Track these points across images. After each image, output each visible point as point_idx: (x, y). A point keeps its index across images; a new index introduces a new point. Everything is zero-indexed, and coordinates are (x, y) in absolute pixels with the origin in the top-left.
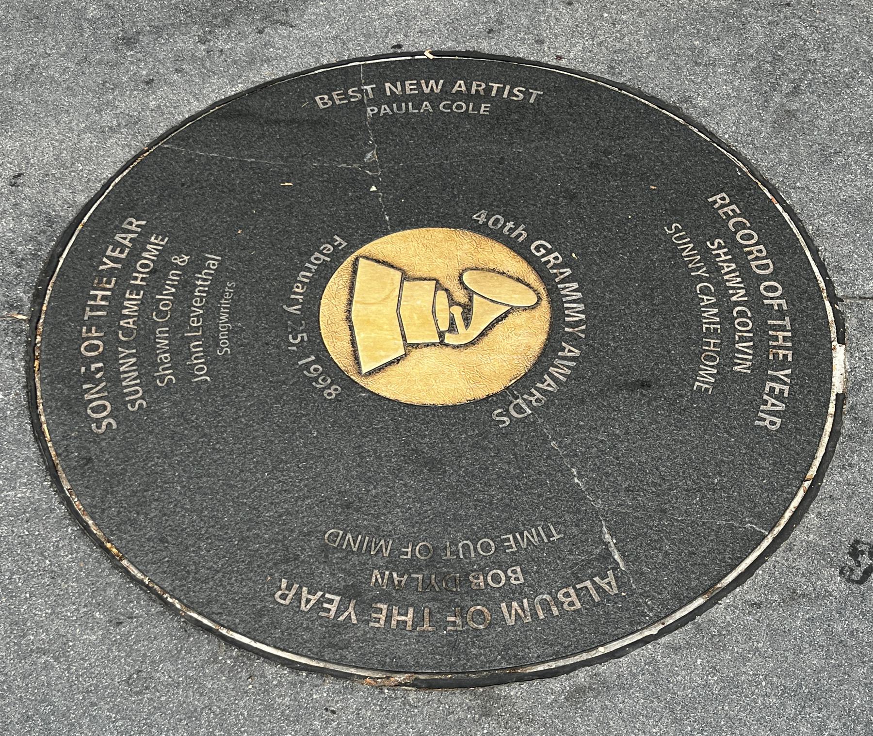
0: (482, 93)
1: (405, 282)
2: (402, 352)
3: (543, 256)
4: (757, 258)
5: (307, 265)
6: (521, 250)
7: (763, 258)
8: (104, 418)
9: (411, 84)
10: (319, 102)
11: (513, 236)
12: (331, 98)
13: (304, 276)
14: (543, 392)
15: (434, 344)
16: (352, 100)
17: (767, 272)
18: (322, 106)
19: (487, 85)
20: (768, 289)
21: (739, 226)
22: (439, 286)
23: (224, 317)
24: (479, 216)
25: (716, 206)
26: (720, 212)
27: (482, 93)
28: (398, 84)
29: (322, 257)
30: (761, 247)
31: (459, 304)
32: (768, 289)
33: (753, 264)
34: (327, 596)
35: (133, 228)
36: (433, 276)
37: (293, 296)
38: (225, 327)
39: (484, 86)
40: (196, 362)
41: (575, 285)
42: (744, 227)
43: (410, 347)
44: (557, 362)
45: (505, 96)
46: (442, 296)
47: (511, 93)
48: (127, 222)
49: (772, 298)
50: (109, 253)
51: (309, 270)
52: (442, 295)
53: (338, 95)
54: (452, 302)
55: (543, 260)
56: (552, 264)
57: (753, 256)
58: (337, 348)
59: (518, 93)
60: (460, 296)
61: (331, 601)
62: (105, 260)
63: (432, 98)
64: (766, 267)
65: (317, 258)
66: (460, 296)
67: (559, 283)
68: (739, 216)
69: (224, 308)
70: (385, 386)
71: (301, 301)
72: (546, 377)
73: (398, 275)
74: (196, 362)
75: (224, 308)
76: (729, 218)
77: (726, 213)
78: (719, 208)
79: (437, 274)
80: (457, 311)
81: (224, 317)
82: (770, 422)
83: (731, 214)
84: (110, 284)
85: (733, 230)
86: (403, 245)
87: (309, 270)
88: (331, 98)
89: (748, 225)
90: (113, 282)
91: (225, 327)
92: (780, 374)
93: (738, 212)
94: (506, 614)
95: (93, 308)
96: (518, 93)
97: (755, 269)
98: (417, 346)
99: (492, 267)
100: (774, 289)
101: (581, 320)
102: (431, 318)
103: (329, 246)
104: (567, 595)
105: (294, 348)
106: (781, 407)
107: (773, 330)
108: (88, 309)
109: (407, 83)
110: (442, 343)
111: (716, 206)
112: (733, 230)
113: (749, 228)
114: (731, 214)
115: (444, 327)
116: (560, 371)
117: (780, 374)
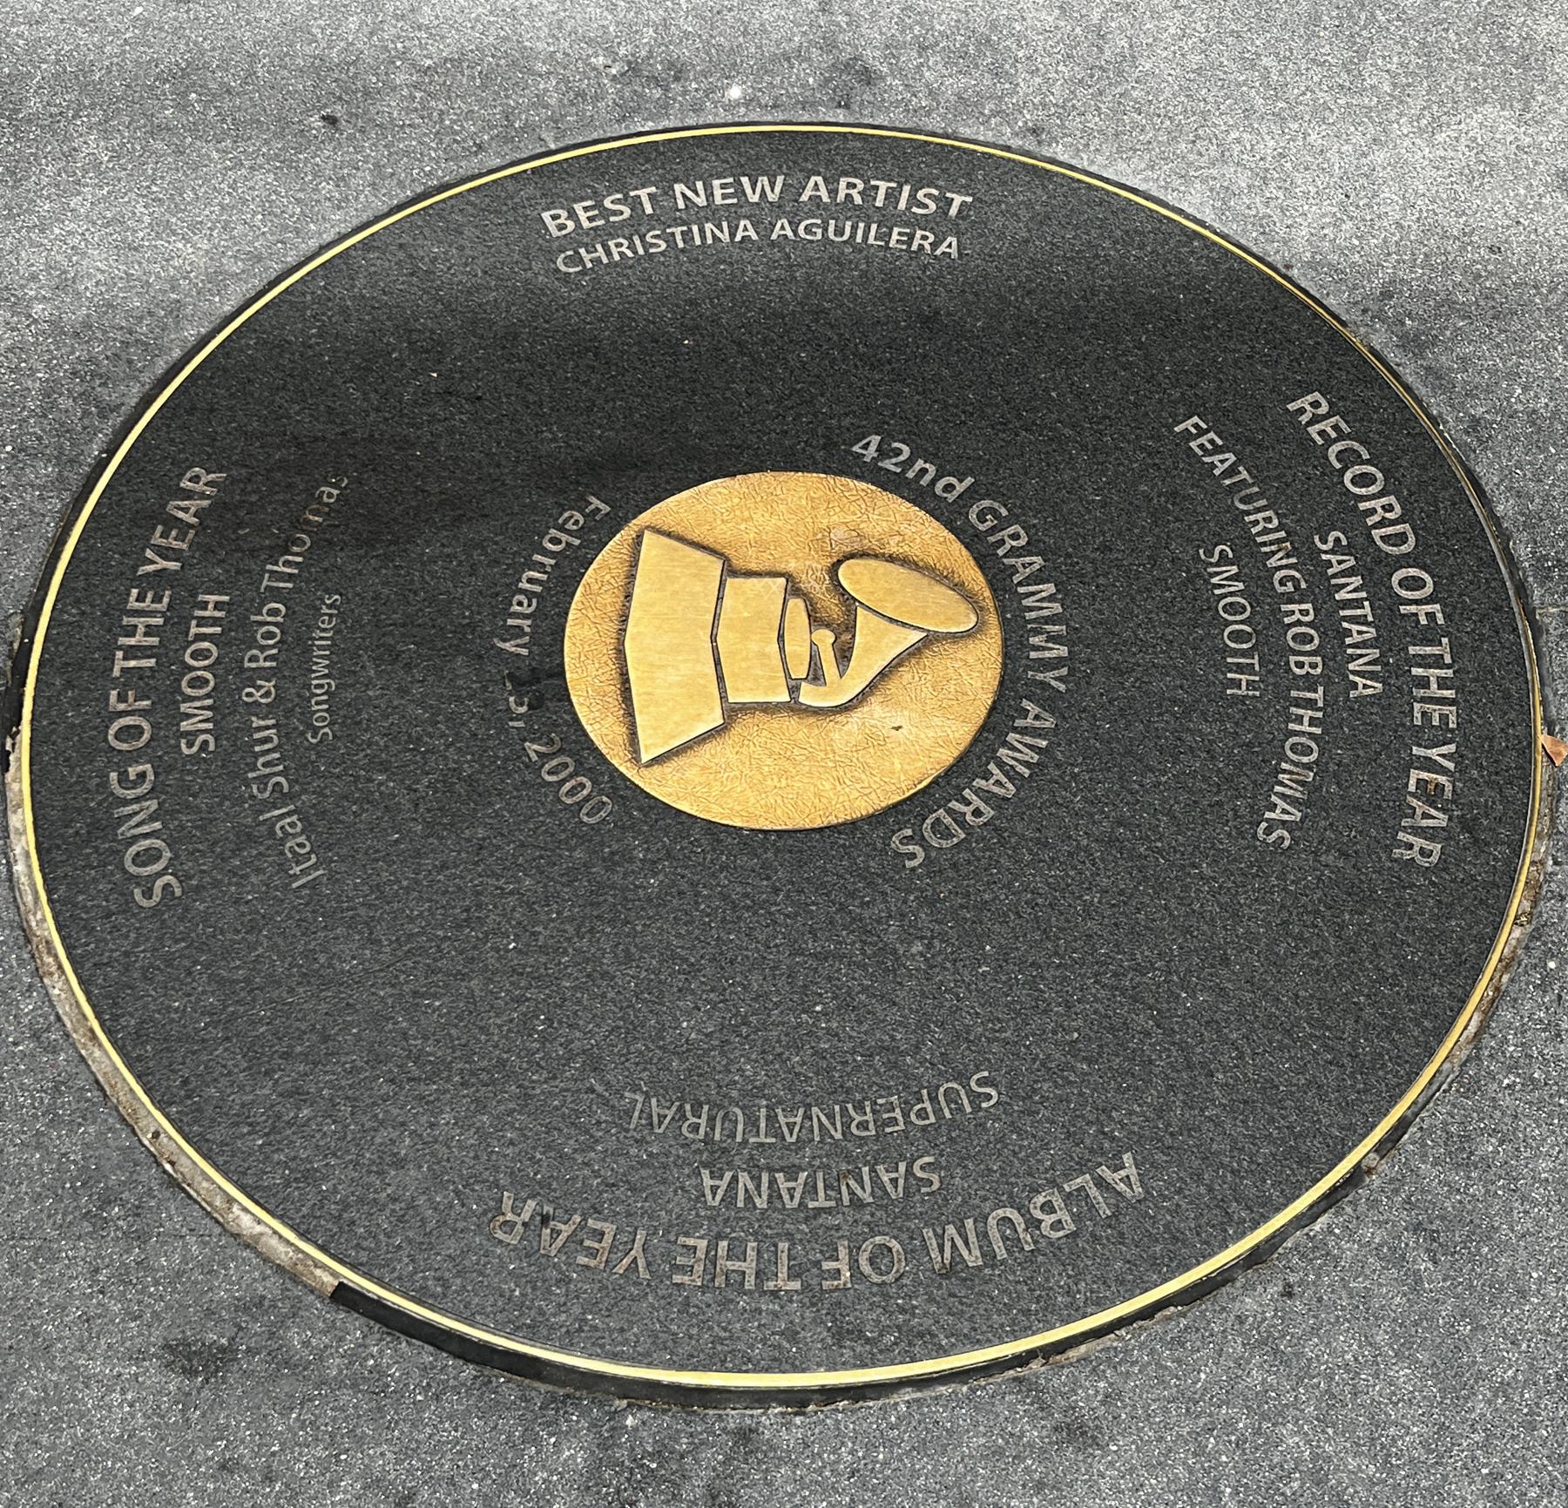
0: (858, 200)
1: (730, 581)
2: (716, 719)
3: (993, 531)
4: (1382, 523)
5: (538, 558)
6: (950, 516)
7: (1393, 523)
8: (160, 874)
9: (723, 186)
10: (551, 225)
11: (910, 475)
12: (572, 215)
13: (530, 581)
14: (988, 797)
15: (767, 708)
16: (612, 219)
17: (1404, 549)
18: (555, 233)
19: (866, 182)
20: (1408, 583)
21: (1349, 458)
22: (794, 589)
23: (321, 666)
24: (866, 447)
25: (1304, 419)
26: (1313, 431)
27: (858, 200)
28: (699, 185)
29: (564, 537)
30: (1392, 499)
31: (828, 626)
32: (1408, 583)
33: (1376, 533)
34: (1200, 453)
35: (199, 487)
36: (781, 567)
37: (510, 622)
38: (322, 686)
39: (861, 186)
40: (268, 771)
41: (1050, 588)
42: (1341, 436)
43: (733, 713)
44: (1012, 737)
45: (902, 205)
46: (797, 606)
47: (975, 1098)
48: (188, 475)
49: (1416, 602)
50: (157, 540)
51: (541, 567)
52: (796, 604)
53: (586, 209)
54: (816, 619)
55: (992, 539)
56: (1008, 546)
57: (1376, 518)
58: (600, 725)
59: (927, 201)
60: (831, 606)
61: (1201, 446)
62: (149, 554)
63: (762, 215)
64: (1401, 538)
65: (556, 541)
66: (831, 606)
67: (1020, 584)
68: (1349, 437)
69: (320, 648)
70: (693, 790)
71: (527, 630)
72: (992, 767)
73: (716, 566)
74: (268, 771)
75: (320, 648)
76: (1329, 442)
77: (1322, 433)
78: (1310, 423)
79: (792, 566)
80: (825, 638)
81: (321, 666)
82: (1417, 848)
83: (1334, 435)
84: (160, 601)
85: (1338, 466)
86: (677, 508)
87: (541, 567)
88: (572, 215)
89: (1366, 456)
90: (166, 600)
91: (322, 686)
92: (1433, 753)
93: (1220, 442)
94: (1047, 654)
95: (130, 653)
96: (927, 201)
97: (1379, 543)
98: (745, 708)
99: (893, 549)
100: (1417, 584)
101: (1060, 658)
102: (765, 658)
103: (578, 516)
104: (1048, 1208)
105: (520, 724)
106: (1441, 820)
107: (1420, 666)
108: (120, 654)
109: (716, 183)
110: (794, 708)
111: (1304, 419)
112: (1338, 466)
113: (1368, 462)
114: (1334, 435)
115: (799, 671)
116: (1019, 752)
117: (1433, 753)
